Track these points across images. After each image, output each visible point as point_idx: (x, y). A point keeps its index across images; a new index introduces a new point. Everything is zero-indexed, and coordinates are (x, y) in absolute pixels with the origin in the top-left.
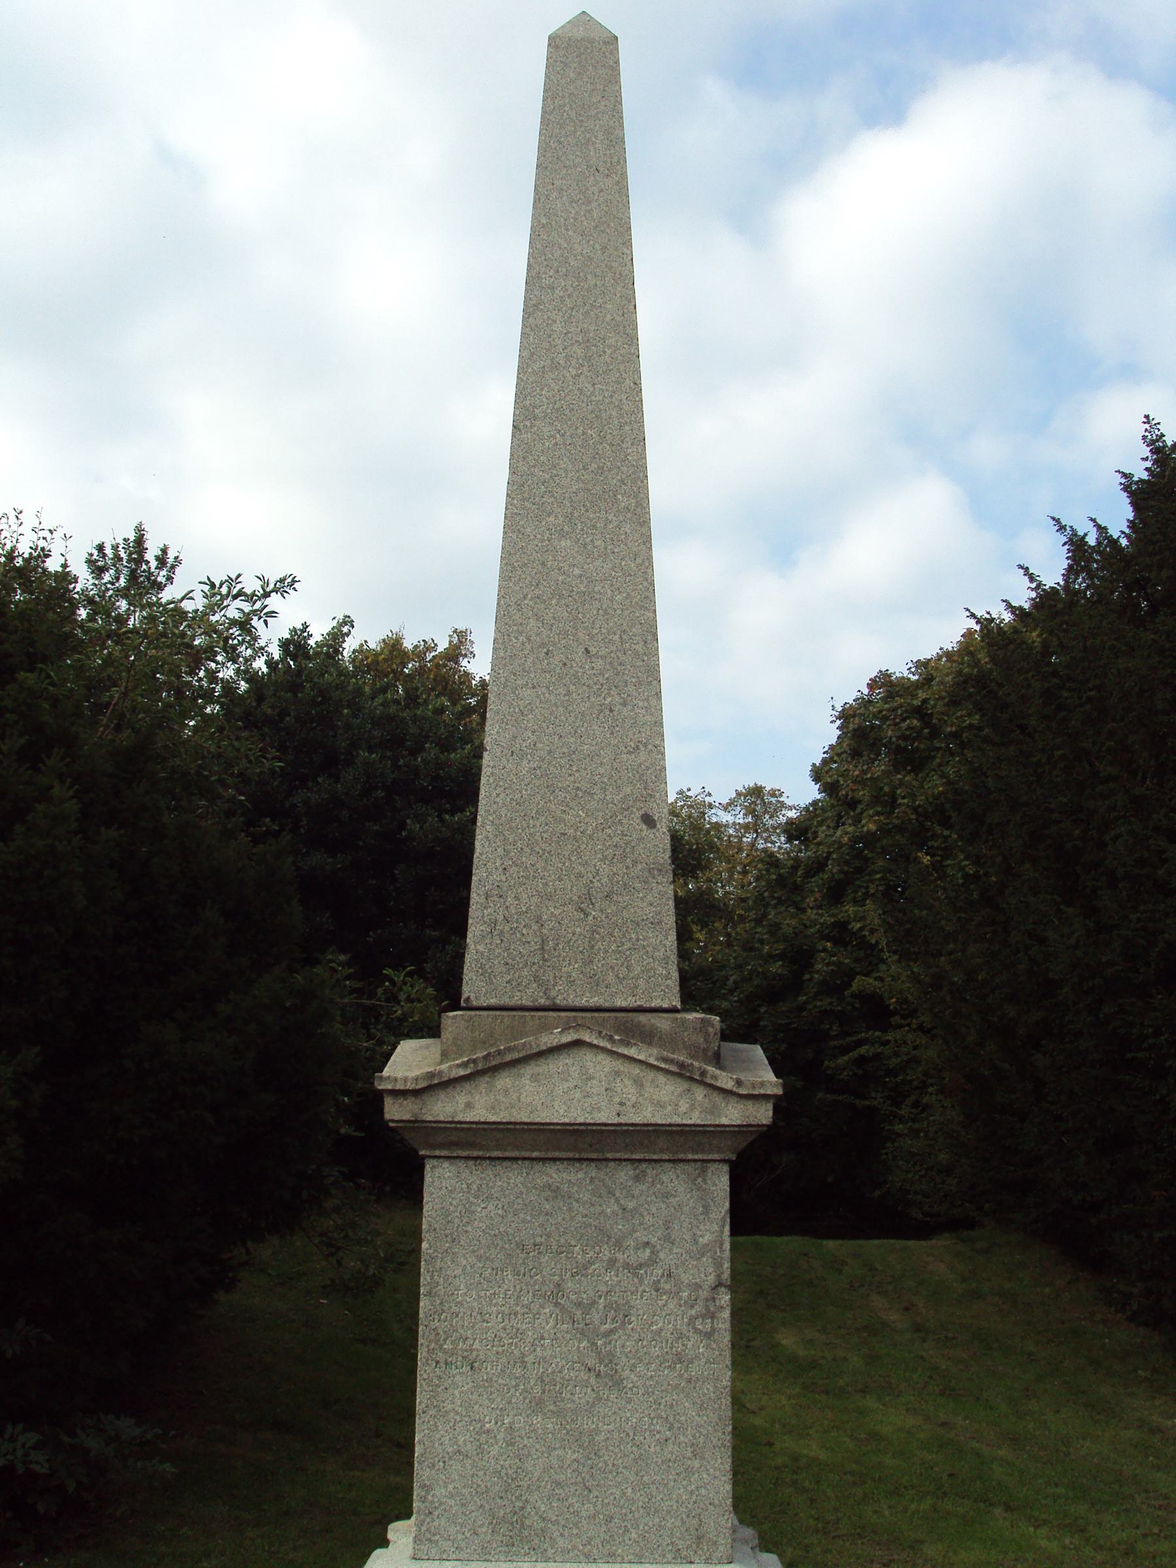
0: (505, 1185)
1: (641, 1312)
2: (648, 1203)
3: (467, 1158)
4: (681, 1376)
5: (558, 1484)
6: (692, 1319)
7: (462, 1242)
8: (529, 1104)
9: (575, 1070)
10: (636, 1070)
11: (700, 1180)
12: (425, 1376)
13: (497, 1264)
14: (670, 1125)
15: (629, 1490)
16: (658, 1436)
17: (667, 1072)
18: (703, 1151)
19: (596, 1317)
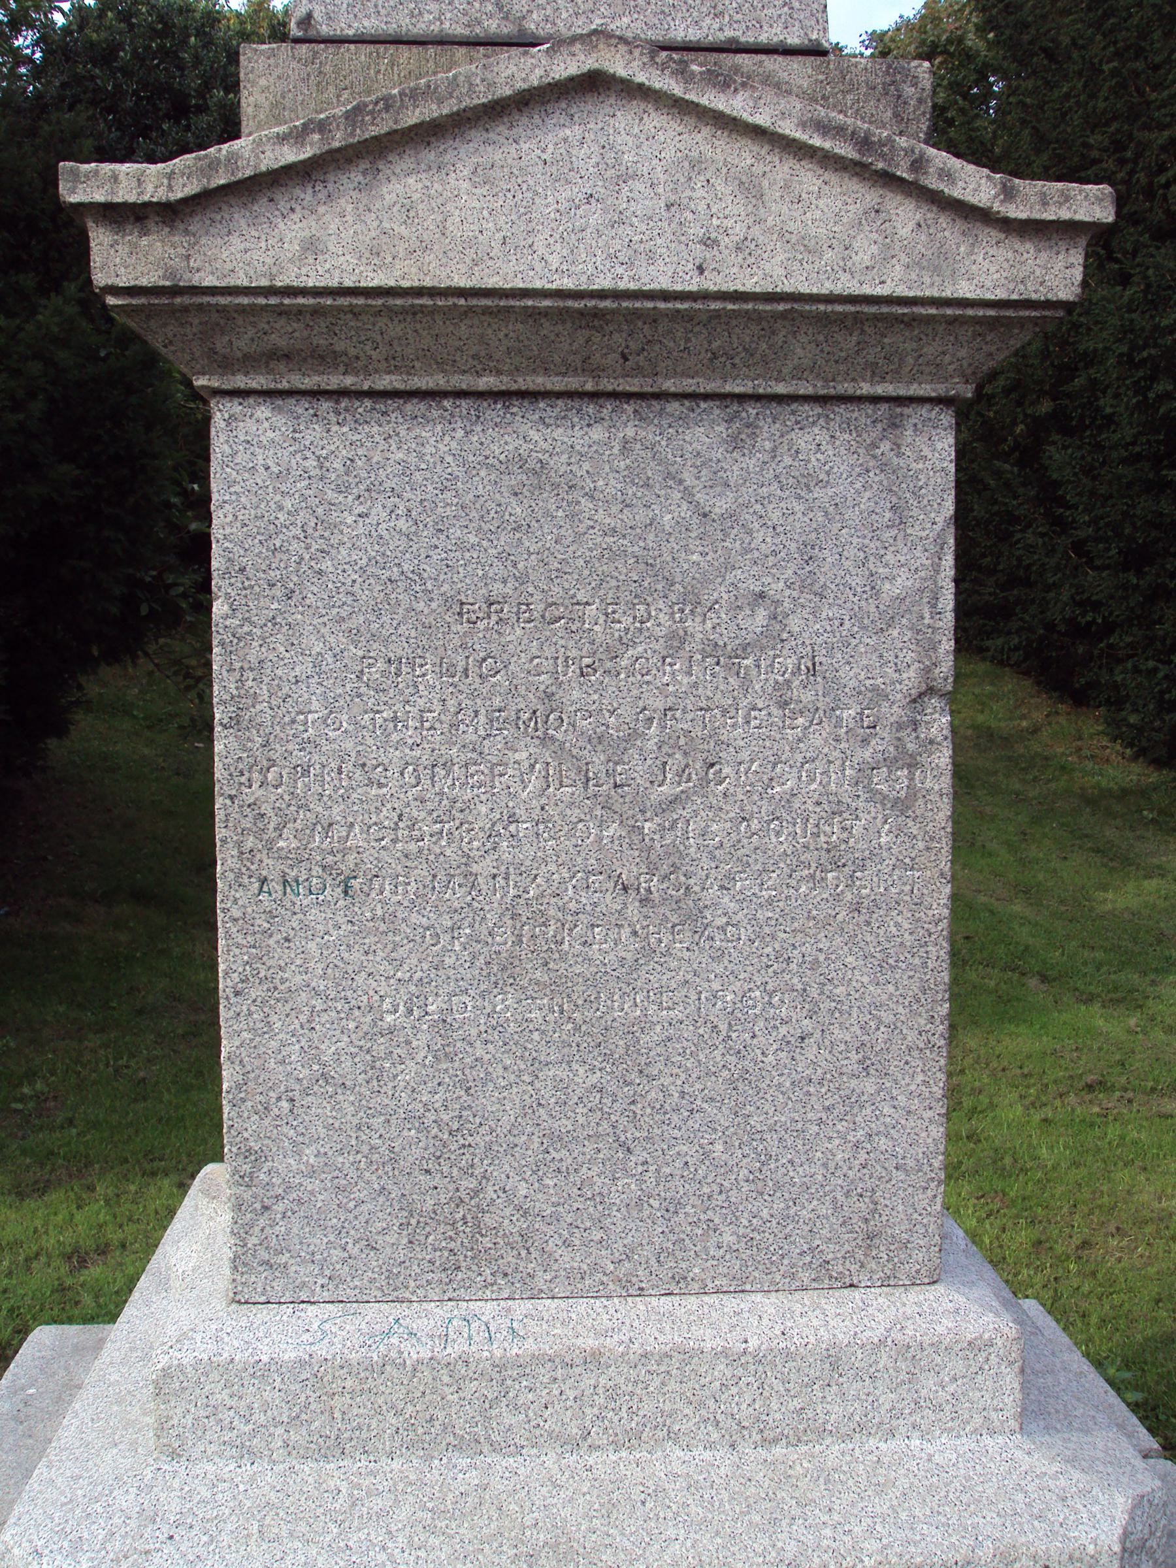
0: (412, 459)
1: (745, 755)
2: (760, 501)
3: (316, 394)
4: (838, 897)
5: (556, 1138)
6: (866, 770)
7: (311, 600)
8: (471, 242)
9: (586, 156)
10: (745, 156)
11: (885, 446)
12: (236, 913)
13: (398, 650)
14: (830, 299)
15: (719, 1147)
16: (783, 1030)
17: (827, 160)
18: (896, 376)
19: (637, 768)
